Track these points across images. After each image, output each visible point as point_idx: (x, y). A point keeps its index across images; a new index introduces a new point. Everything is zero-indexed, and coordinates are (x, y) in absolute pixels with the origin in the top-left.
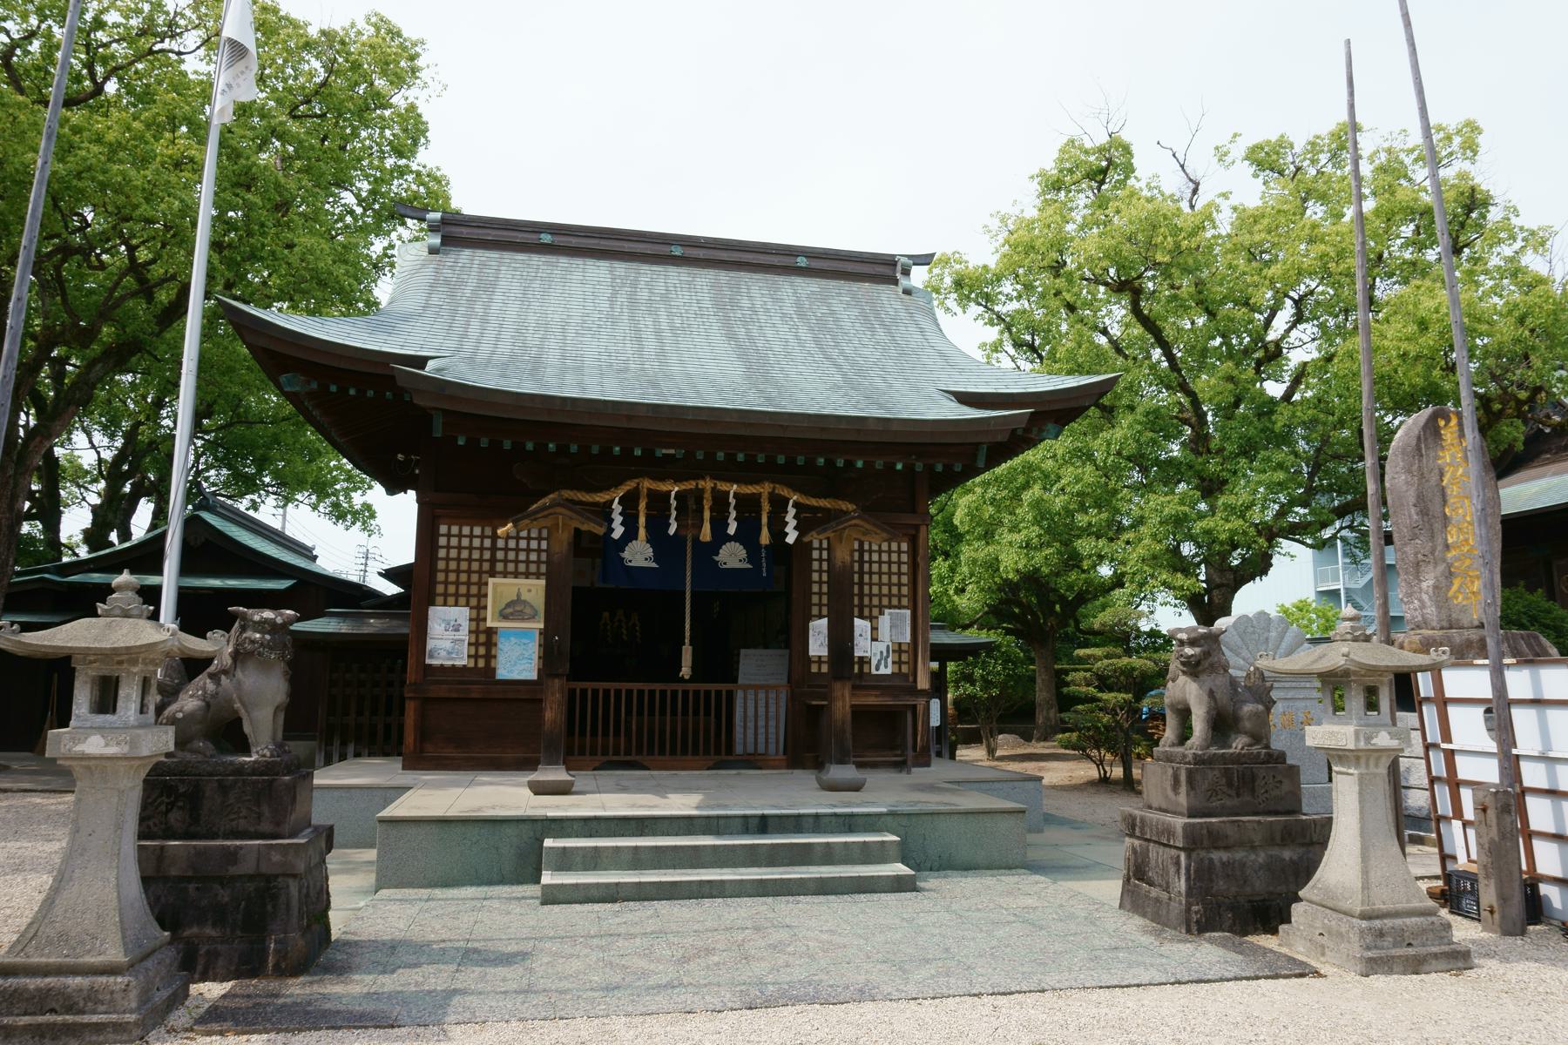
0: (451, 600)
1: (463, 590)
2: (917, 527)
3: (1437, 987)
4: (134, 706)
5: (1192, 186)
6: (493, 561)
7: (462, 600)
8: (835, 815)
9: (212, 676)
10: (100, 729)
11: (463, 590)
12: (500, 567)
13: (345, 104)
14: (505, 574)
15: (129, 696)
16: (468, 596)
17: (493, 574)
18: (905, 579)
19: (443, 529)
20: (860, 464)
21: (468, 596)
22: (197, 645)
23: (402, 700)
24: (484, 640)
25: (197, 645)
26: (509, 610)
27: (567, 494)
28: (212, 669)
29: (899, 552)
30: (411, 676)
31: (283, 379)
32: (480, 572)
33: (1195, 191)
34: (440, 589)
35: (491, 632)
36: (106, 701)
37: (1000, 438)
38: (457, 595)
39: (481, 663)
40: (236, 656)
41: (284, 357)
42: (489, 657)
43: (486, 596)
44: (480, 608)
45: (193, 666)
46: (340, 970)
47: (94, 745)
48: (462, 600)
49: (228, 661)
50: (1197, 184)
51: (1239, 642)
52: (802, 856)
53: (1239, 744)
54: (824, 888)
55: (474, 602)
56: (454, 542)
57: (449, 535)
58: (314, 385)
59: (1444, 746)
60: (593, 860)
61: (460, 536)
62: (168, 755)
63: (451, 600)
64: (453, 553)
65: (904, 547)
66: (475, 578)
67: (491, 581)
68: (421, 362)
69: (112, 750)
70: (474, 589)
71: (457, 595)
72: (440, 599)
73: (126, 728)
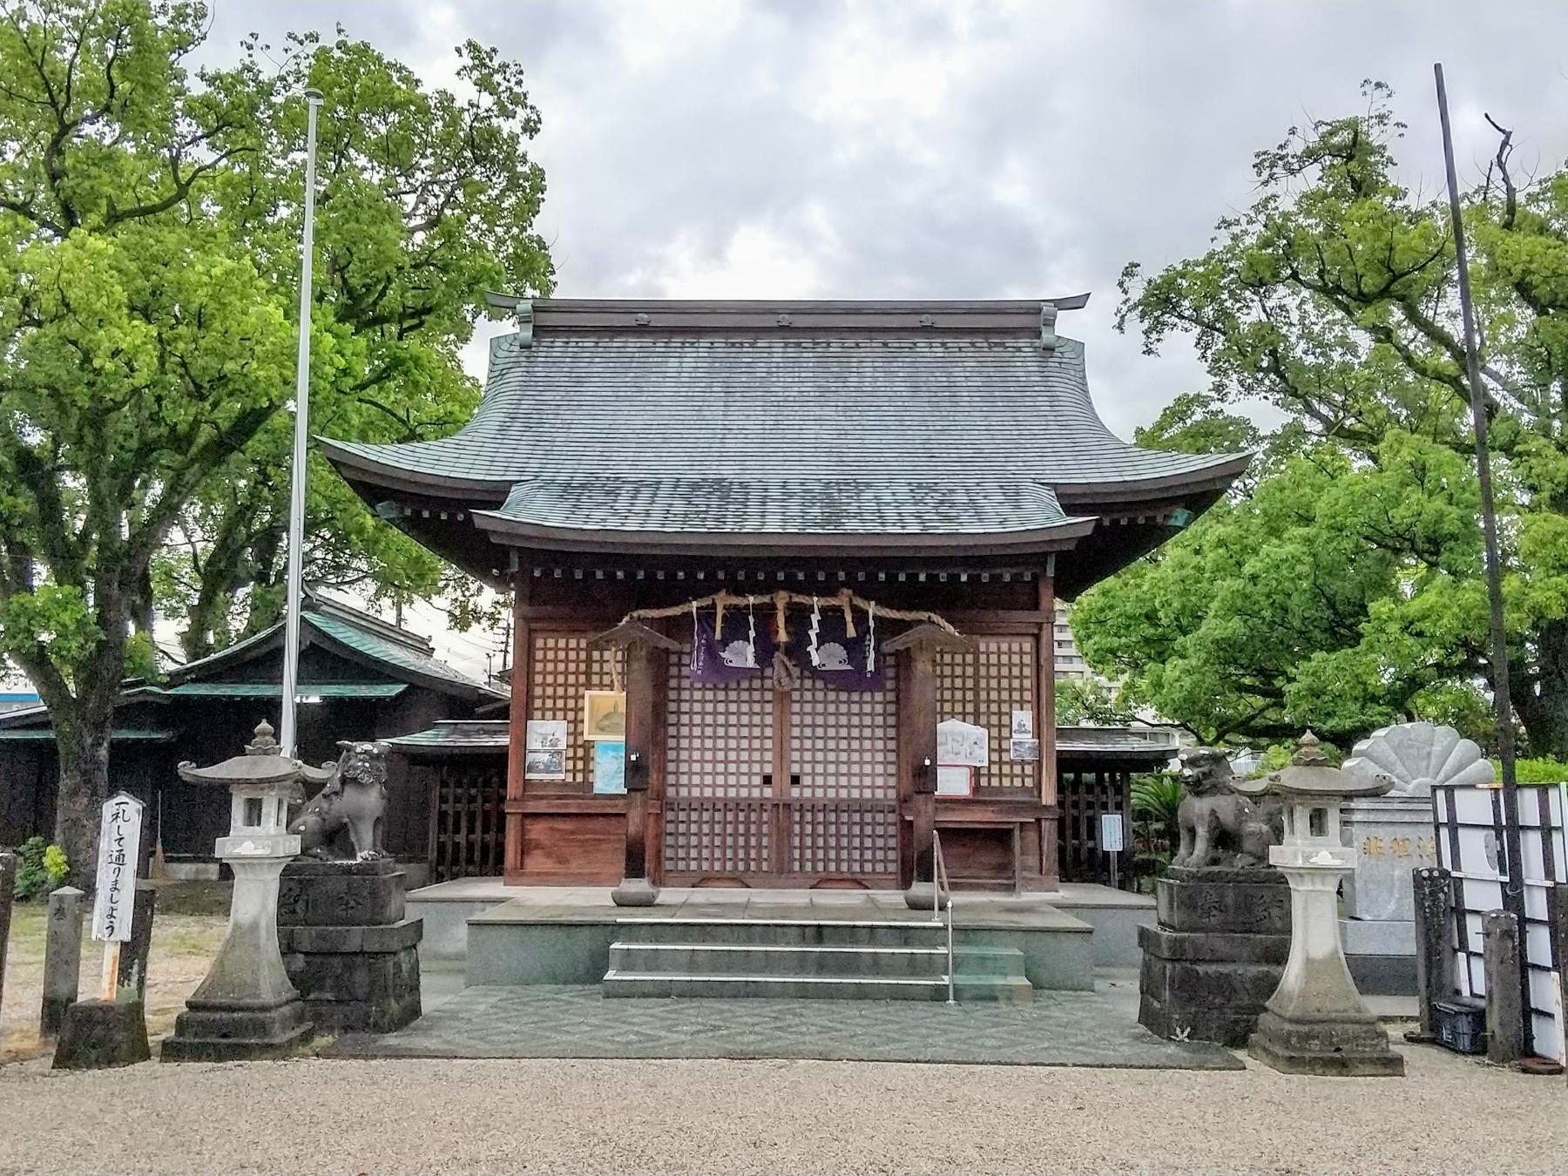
0: (549, 714)
1: (560, 703)
2: (1040, 626)
3: (1359, 1088)
4: (273, 820)
5: (1503, 137)
6: (588, 674)
7: (560, 714)
8: (890, 927)
9: (325, 796)
10: (250, 837)
11: (560, 703)
12: (595, 679)
13: (422, 201)
14: (601, 686)
15: (269, 809)
16: (565, 709)
17: (589, 685)
18: (1027, 683)
19: (539, 643)
20: (922, 578)
21: (565, 709)
22: (313, 773)
23: (502, 816)
24: (583, 753)
25: (313, 773)
26: (606, 723)
27: (642, 613)
28: (326, 791)
29: (1022, 653)
30: (512, 790)
31: (379, 507)
32: (576, 685)
33: (1505, 144)
34: (538, 703)
35: (588, 746)
36: (254, 812)
37: (1065, 547)
38: (554, 710)
39: (580, 778)
40: (344, 781)
41: (374, 488)
42: (587, 771)
43: (582, 709)
44: (577, 722)
45: (312, 789)
46: (426, 1031)
47: (247, 849)
48: (560, 714)
49: (338, 786)
50: (1508, 135)
51: (1393, 757)
52: (849, 964)
53: (1241, 862)
54: (861, 994)
55: (571, 715)
56: (551, 655)
57: (545, 649)
58: (408, 512)
59: (1454, 874)
60: (653, 962)
61: (556, 649)
62: (296, 858)
63: (549, 714)
64: (572, 655)
65: (1027, 647)
66: (571, 691)
67: (587, 693)
68: (495, 495)
69: (260, 852)
70: (571, 703)
71: (554, 710)
72: (538, 714)
73: (269, 837)
